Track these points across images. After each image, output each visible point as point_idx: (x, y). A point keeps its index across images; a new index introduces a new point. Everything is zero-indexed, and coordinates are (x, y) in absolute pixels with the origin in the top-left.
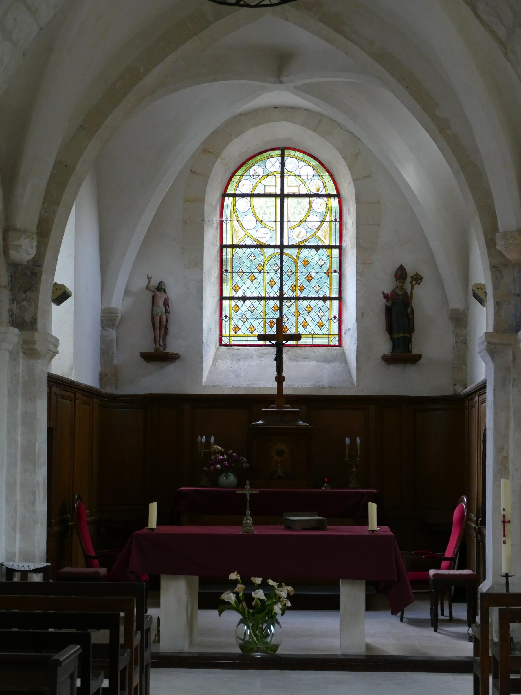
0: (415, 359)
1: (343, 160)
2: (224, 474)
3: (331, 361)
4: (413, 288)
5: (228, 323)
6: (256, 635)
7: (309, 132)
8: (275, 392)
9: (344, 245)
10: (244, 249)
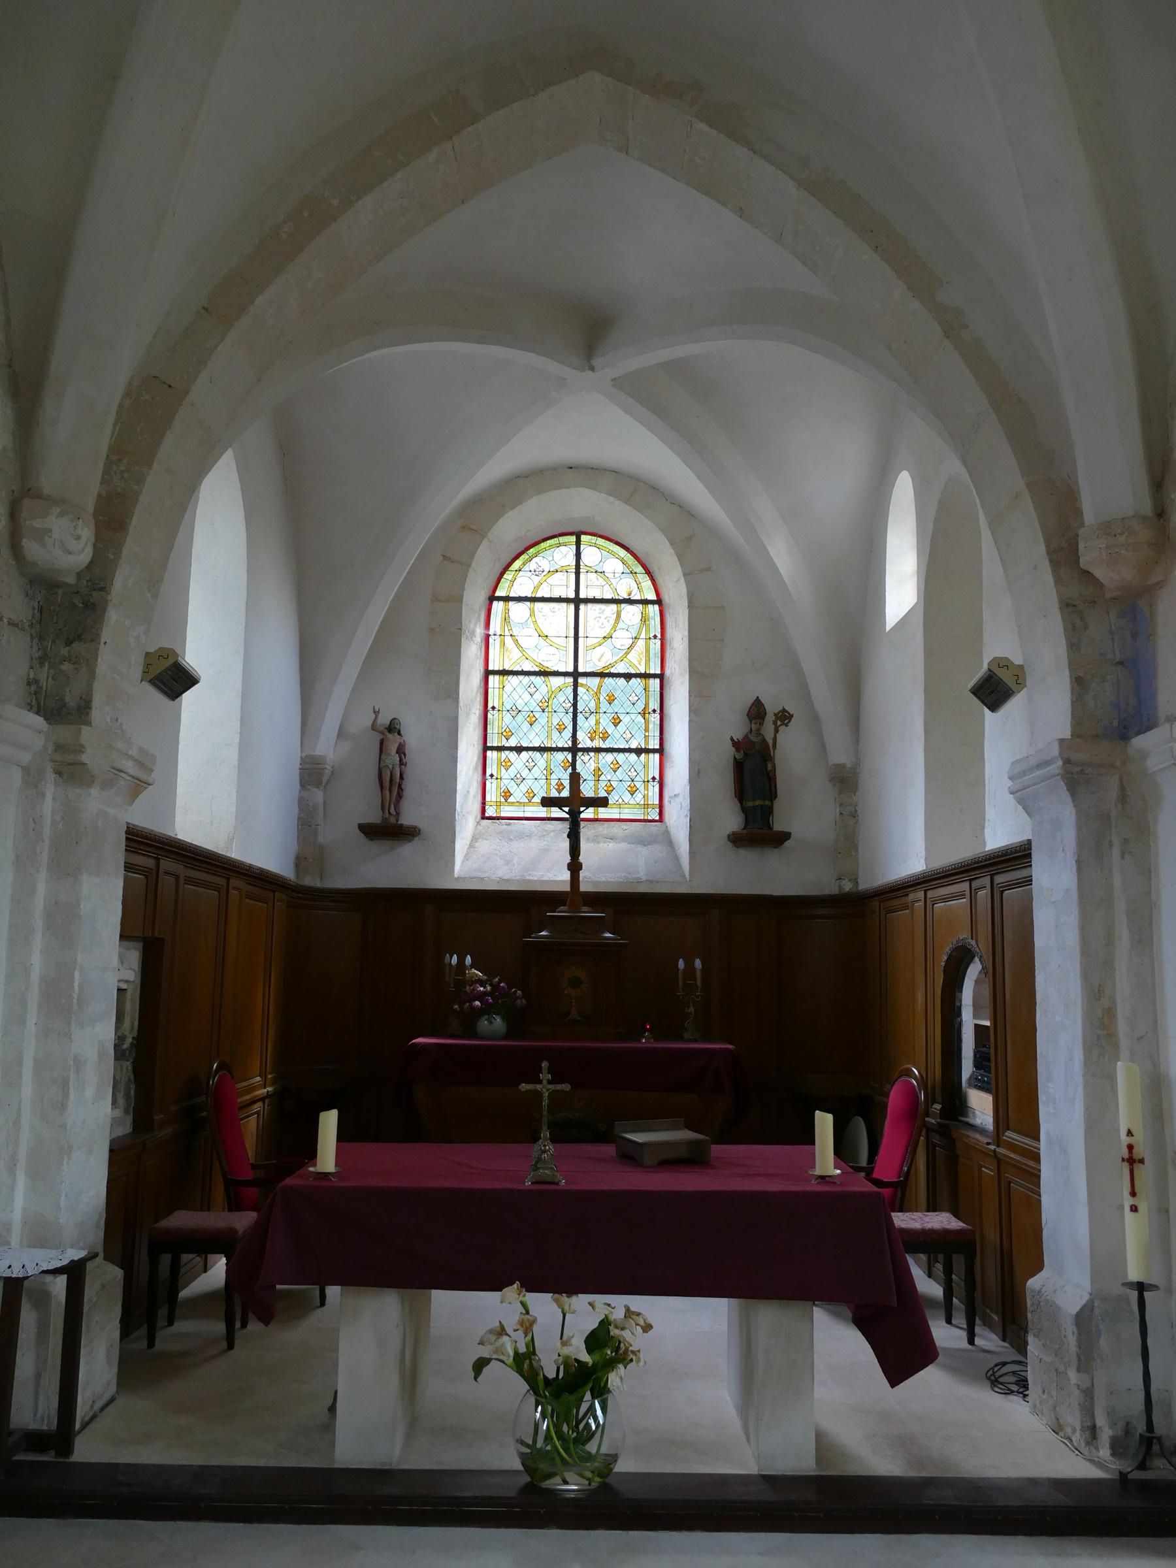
1: (668, 544)
3: (649, 843)
4: (777, 731)
6: (561, 1437)
7: (619, 505)
8: (568, 888)
9: (668, 672)
10: (521, 677)
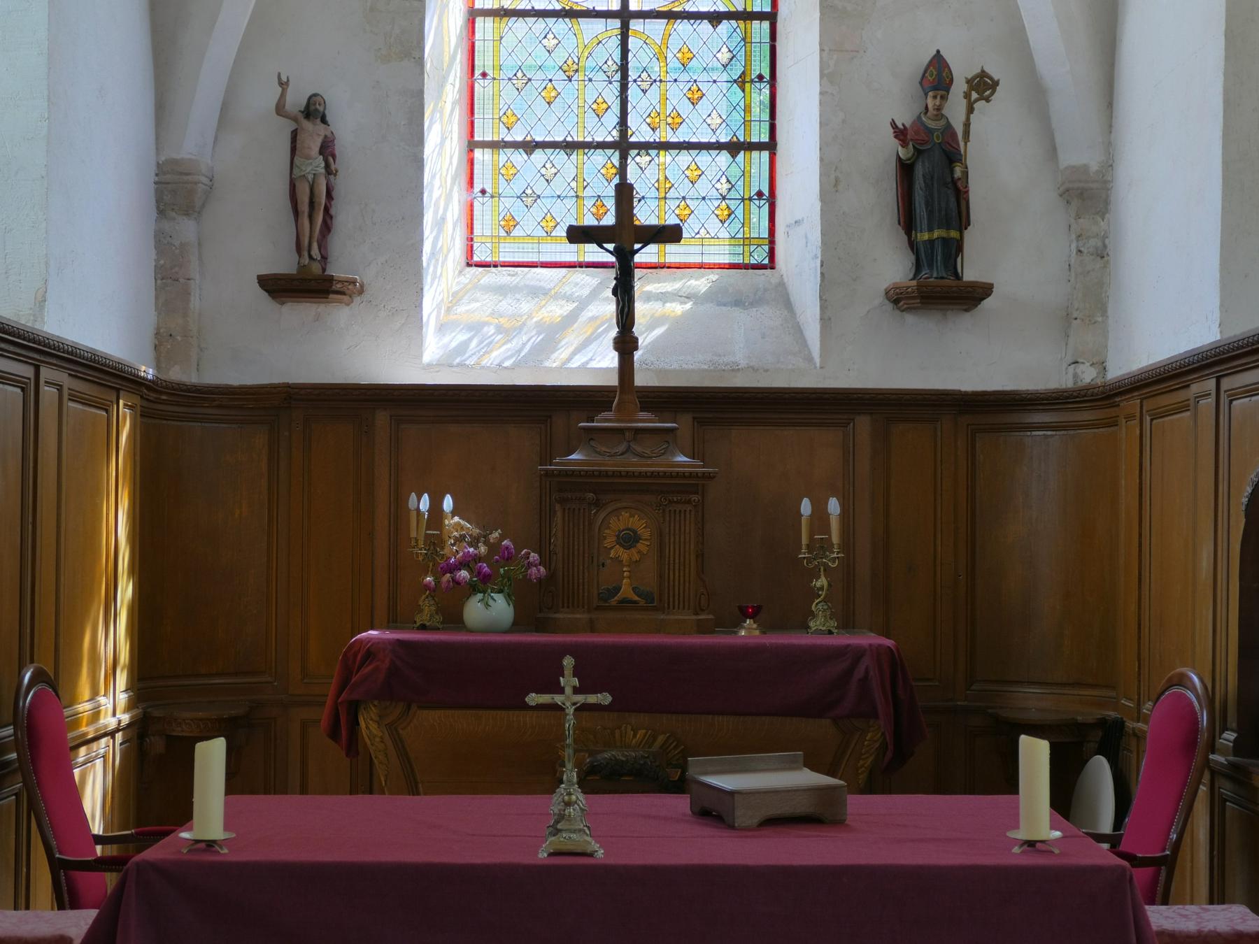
0: (972, 296)
2: (480, 596)
3: (753, 304)
4: (970, 110)
5: (487, 207)
8: (613, 381)
